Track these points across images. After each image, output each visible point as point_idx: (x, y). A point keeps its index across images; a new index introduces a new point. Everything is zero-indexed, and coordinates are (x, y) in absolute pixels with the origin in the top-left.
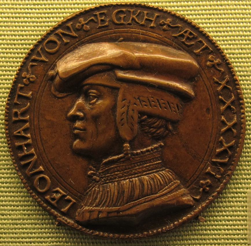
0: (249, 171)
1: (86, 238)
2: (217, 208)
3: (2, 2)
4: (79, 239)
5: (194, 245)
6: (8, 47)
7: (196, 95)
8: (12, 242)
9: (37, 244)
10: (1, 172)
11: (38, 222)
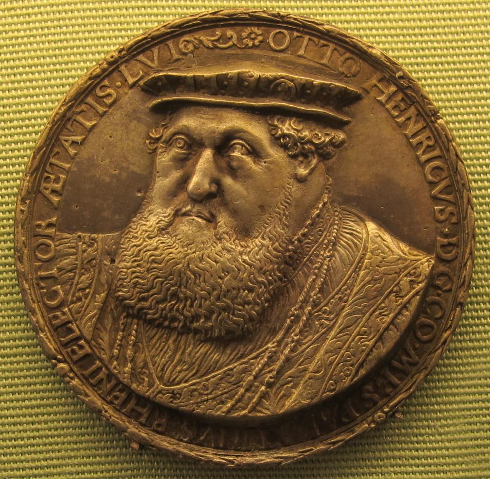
0: (487, 199)
1: (196, 468)
2: (456, 373)
3: (2, 6)
4: (190, 471)
5: (38, 478)
6: (24, 124)
7: (35, 252)
8: (421, 473)
9: (87, 475)
10: (1, 330)
11: (116, 452)
